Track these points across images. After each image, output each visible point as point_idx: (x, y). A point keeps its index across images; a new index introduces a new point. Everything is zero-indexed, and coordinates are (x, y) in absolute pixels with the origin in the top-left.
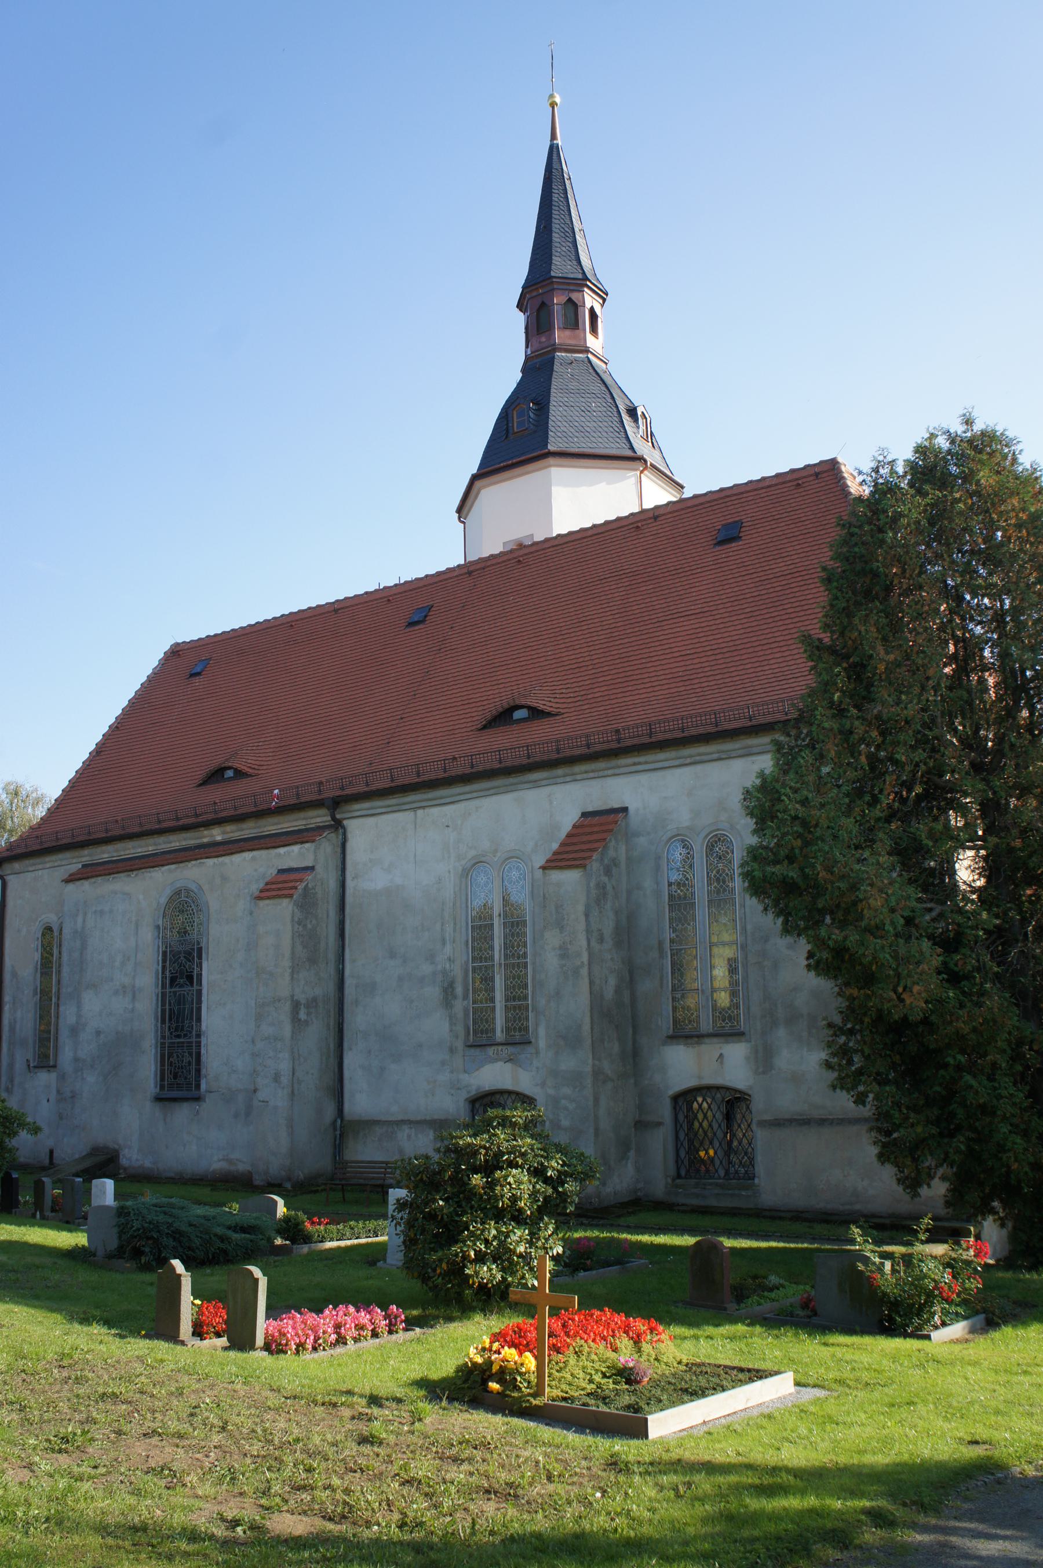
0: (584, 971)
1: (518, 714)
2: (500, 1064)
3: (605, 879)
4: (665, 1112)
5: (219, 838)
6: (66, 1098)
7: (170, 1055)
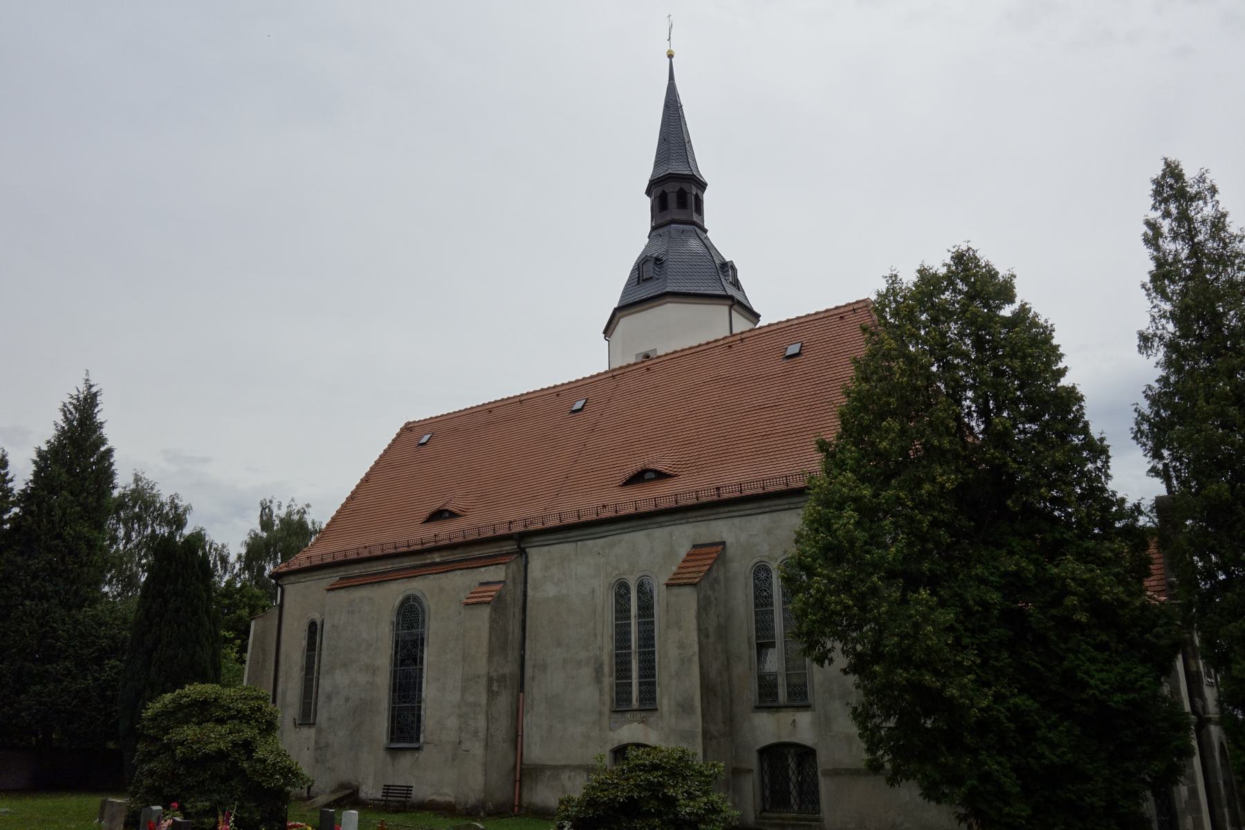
0: (696, 659)
1: (647, 476)
2: (320, 485)
3: (710, 593)
4: (753, 762)
5: (438, 560)
6: (321, 748)
7: (399, 715)
